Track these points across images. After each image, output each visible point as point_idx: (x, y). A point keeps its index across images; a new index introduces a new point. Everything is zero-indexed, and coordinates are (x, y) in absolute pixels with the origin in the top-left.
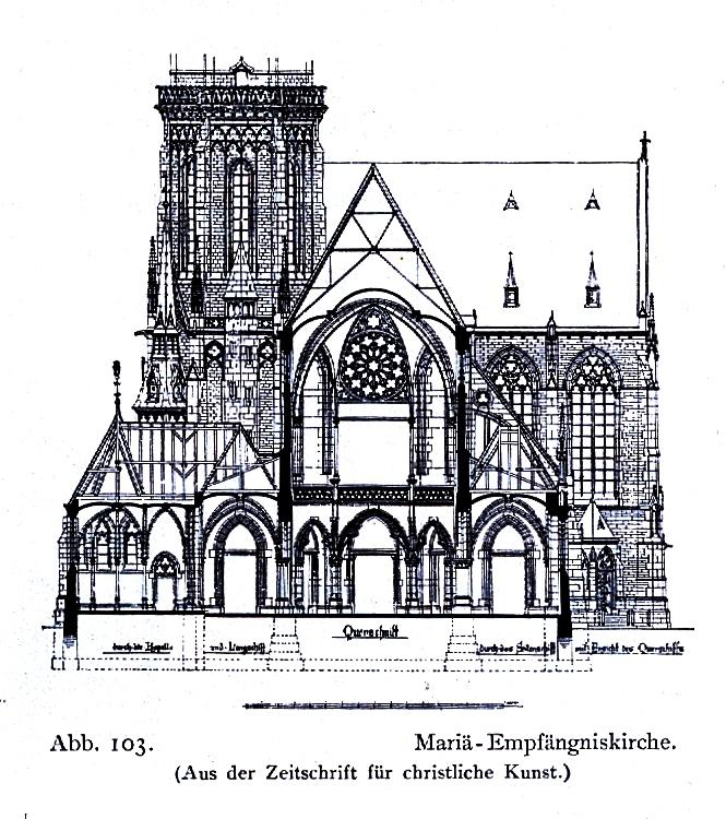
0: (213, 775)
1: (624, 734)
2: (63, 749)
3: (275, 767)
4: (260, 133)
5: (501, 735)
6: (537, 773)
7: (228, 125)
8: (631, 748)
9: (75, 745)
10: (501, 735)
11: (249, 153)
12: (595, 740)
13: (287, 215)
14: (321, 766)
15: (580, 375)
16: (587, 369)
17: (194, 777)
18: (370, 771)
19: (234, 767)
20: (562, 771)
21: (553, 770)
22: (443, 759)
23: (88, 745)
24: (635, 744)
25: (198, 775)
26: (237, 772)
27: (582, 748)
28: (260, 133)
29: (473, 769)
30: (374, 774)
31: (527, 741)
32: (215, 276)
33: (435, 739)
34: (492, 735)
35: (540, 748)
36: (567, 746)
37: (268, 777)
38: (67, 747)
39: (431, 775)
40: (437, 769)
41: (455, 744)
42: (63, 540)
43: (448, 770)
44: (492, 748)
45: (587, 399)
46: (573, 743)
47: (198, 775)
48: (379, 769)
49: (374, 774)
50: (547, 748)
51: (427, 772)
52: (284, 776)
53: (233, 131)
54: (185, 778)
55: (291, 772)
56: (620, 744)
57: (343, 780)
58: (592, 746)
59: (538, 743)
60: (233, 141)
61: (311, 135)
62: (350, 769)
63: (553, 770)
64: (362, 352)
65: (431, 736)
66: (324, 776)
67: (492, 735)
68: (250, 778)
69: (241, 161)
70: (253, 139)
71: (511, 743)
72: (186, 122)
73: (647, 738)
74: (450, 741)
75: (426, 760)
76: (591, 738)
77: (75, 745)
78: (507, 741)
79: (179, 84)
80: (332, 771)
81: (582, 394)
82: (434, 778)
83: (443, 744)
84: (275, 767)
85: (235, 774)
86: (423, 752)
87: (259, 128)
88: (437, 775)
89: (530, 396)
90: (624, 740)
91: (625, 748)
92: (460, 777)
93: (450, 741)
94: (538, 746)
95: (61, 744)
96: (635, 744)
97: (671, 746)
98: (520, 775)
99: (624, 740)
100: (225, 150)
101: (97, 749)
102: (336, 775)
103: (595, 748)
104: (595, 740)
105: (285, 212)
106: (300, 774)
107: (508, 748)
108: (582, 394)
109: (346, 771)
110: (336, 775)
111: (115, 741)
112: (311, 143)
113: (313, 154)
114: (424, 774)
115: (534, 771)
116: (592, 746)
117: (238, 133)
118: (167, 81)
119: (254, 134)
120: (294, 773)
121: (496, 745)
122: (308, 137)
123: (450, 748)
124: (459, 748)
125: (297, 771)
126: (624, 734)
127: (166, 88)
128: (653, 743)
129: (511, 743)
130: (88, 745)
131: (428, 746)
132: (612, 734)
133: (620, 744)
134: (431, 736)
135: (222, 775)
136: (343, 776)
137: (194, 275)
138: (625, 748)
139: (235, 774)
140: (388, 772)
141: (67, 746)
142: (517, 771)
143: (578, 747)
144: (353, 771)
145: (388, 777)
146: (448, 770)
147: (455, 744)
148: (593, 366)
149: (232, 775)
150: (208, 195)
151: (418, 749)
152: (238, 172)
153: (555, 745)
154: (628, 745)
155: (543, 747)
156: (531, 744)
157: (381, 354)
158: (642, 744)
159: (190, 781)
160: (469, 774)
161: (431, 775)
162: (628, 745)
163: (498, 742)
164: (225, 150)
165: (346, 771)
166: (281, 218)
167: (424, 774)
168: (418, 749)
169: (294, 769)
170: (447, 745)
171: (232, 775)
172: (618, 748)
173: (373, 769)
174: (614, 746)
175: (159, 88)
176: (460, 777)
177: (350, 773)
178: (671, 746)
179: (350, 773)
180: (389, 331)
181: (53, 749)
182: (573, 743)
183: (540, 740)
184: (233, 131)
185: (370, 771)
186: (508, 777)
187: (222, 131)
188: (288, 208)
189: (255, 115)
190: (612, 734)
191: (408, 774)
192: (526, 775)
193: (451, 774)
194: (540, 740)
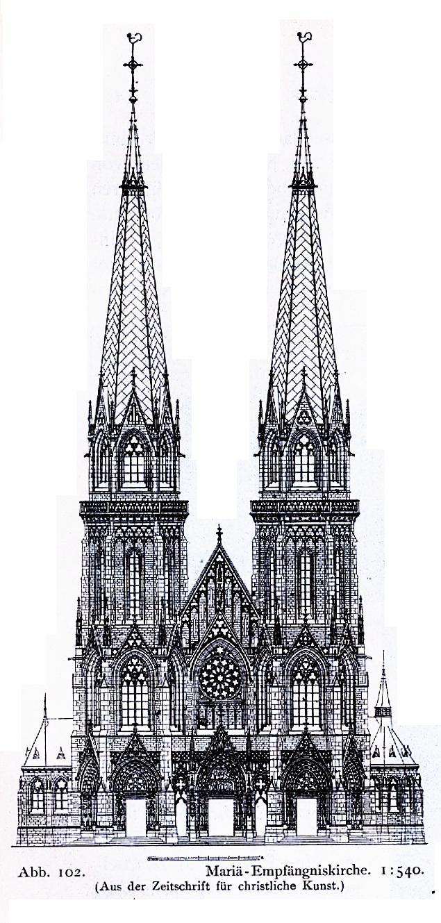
0: (119, 887)
1: (338, 865)
2: (293, 874)
3: (158, 882)
4: (126, 531)
5: (260, 866)
6: (323, 886)
7: (307, 525)
8: (342, 874)
9: (34, 873)
10: (260, 866)
11: (139, 544)
12: (320, 869)
13: (335, 582)
14: (246, 882)
15: (126, 673)
16: (131, 668)
17: (27, 876)
18: (218, 885)
19: (132, 882)
20: (339, 885)
21: (333, 884)
22: (265, 880)
23: (43, 873)
24: (345, 872)
25: (109, 888)
26: (134, 886)
27: (312, 874)
28: (146, 531)
29: (185, 884)
30: (220, 888)
31: (276, 870)
32: (118, 622)
33: (219, 869)
34: (254, 867)
35: (285, 874)
36: (302, 873)
37: (154, 889)
38: (29, 874)
39: (256, 887)
40: (260, 884)
41: (231, 873)
42: (418, 778)
43: (267, 885)
44: (254, 875)
45: (132, 690)
46: (306, 871)
47: (109, 888)
48: (223, 884)
49: (220, 888)
50: (289, 874)
51: (253, 885)
52: (364, 872)
53: (320, 530)
54: (102, 890)
55: (199, 886)
56: (336, 872)
57: (201, 891)
58: (318, 873)
59: (283, 871)
60: (139, 537)
61: (349, 531)
62: (205, 884)
63: (333, 884)
64: (212, 669)
65: (216, 867)
66: (248, 888)
67: (254, 867)
68: (143, 889)
69: (134, 549)
70: (142, 535)
71: (266, 871)
72: (94, 524)
73: (352, 867)
74: (228, 871)
75: (213, 881)
76: (317, 868)
77: (34, 873)
78: (264, 870)
79: (95, 500)
80: (194, 886)
81: (299, 686)
82: (258, 889)
83: (224, 872)
84: (158, 882)
85: (132, 887)
86: (212, 877)
87: (307, 527)
88: (260, 888)
89: (318, 687)
90: (338, 869)
91: (338, 874)
92: (275, 889)
93: (228, 871)
94: (283, 873)
95: (25, 873)
96: (345, 872)
97: (367, 872)
98: (312, 887)
99: (338, 869)
100: (124, 543)
101: (49, 876)
102: (197, 888)
103: (320, 874)
104: (320, 869)
105: (334, 580)
106: (173, 887)
107: (264, 875)
108: (299, 686)
109: (203, 885)
110: (197, 888)
111: (61, 870)
112: (179, 538)
113: (179, 543)
114: (251, 887)
115: (321, 885)
116: (318, 873)
117: (132, 531)
118: (257, 497)
119: (132, 531)
120: (170, 887)
121: (257, 873)
122: (347, 533)
123: (228, 875)
124: (234, 875)
125: (172, 885)
126: (338, 865)
127: (86, 502)
128: (356, 870)
129: (266, 871)
130: (43, 873)
131: (214, 874)
132: (330, 866)
133: (336, 872)
134: (216, 867)
135: (124, 887)
136: (201, 888)
137: (105, 622)
138: (338, 874)
139: (132, 887)
140: (229, 886)
141: (29, 874)
142: (311, 885)
143: (309, 874)
144: (207, 885)
145: (229, 889)
146: (267, 885)
147: (231, 873)
148: (135, 666)
149: (131, 888)
150: (113, 571)
151: (208, 875)
152: (132, 556)
153: (294, 873)
154: (340, 872)
155: (287, 873)
156: (279, 872)
157: (225, 670)
158: (350, 872)
159: (105, 891)
160: (280, 887)
161: (256, 887)
162: (340, 872)
163: (258, 870)
164: (124, 543)
165: (203, 885)
166: (331, 584)
167: (251, 887)
168: (208, 875)
169: (169, 884)
170: (226, 873)
171: (131, 888)
172: (334, 874)
173: (220, 884)
174: (331, 873)
175: (252, 502)
176: (275, 889)
177: (205, 887)
178: (367, 872)
179: (205, 887)
180: (229, 656)
181: (20, 876)
182: (306, 871)
183: (285, 869)
184: (139, 530)
185: (218, 885)
186: (305, 888)
187: (122, 530)
188: (336, 578)
189: (291, 519)
190: (330, 866)
191: (241, 887)
192: (316, 888)
193: (269, 887)
194: (285, 869)
